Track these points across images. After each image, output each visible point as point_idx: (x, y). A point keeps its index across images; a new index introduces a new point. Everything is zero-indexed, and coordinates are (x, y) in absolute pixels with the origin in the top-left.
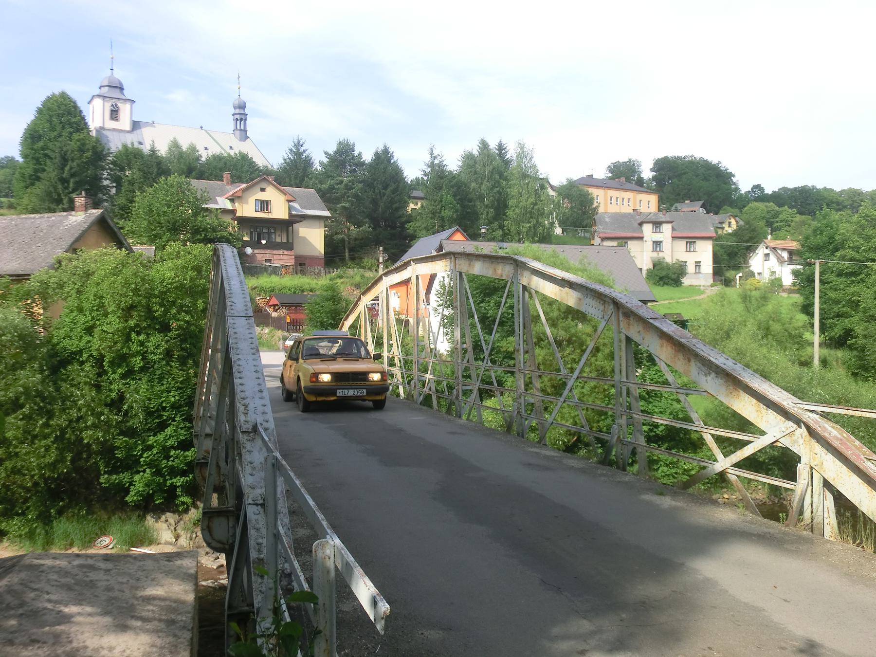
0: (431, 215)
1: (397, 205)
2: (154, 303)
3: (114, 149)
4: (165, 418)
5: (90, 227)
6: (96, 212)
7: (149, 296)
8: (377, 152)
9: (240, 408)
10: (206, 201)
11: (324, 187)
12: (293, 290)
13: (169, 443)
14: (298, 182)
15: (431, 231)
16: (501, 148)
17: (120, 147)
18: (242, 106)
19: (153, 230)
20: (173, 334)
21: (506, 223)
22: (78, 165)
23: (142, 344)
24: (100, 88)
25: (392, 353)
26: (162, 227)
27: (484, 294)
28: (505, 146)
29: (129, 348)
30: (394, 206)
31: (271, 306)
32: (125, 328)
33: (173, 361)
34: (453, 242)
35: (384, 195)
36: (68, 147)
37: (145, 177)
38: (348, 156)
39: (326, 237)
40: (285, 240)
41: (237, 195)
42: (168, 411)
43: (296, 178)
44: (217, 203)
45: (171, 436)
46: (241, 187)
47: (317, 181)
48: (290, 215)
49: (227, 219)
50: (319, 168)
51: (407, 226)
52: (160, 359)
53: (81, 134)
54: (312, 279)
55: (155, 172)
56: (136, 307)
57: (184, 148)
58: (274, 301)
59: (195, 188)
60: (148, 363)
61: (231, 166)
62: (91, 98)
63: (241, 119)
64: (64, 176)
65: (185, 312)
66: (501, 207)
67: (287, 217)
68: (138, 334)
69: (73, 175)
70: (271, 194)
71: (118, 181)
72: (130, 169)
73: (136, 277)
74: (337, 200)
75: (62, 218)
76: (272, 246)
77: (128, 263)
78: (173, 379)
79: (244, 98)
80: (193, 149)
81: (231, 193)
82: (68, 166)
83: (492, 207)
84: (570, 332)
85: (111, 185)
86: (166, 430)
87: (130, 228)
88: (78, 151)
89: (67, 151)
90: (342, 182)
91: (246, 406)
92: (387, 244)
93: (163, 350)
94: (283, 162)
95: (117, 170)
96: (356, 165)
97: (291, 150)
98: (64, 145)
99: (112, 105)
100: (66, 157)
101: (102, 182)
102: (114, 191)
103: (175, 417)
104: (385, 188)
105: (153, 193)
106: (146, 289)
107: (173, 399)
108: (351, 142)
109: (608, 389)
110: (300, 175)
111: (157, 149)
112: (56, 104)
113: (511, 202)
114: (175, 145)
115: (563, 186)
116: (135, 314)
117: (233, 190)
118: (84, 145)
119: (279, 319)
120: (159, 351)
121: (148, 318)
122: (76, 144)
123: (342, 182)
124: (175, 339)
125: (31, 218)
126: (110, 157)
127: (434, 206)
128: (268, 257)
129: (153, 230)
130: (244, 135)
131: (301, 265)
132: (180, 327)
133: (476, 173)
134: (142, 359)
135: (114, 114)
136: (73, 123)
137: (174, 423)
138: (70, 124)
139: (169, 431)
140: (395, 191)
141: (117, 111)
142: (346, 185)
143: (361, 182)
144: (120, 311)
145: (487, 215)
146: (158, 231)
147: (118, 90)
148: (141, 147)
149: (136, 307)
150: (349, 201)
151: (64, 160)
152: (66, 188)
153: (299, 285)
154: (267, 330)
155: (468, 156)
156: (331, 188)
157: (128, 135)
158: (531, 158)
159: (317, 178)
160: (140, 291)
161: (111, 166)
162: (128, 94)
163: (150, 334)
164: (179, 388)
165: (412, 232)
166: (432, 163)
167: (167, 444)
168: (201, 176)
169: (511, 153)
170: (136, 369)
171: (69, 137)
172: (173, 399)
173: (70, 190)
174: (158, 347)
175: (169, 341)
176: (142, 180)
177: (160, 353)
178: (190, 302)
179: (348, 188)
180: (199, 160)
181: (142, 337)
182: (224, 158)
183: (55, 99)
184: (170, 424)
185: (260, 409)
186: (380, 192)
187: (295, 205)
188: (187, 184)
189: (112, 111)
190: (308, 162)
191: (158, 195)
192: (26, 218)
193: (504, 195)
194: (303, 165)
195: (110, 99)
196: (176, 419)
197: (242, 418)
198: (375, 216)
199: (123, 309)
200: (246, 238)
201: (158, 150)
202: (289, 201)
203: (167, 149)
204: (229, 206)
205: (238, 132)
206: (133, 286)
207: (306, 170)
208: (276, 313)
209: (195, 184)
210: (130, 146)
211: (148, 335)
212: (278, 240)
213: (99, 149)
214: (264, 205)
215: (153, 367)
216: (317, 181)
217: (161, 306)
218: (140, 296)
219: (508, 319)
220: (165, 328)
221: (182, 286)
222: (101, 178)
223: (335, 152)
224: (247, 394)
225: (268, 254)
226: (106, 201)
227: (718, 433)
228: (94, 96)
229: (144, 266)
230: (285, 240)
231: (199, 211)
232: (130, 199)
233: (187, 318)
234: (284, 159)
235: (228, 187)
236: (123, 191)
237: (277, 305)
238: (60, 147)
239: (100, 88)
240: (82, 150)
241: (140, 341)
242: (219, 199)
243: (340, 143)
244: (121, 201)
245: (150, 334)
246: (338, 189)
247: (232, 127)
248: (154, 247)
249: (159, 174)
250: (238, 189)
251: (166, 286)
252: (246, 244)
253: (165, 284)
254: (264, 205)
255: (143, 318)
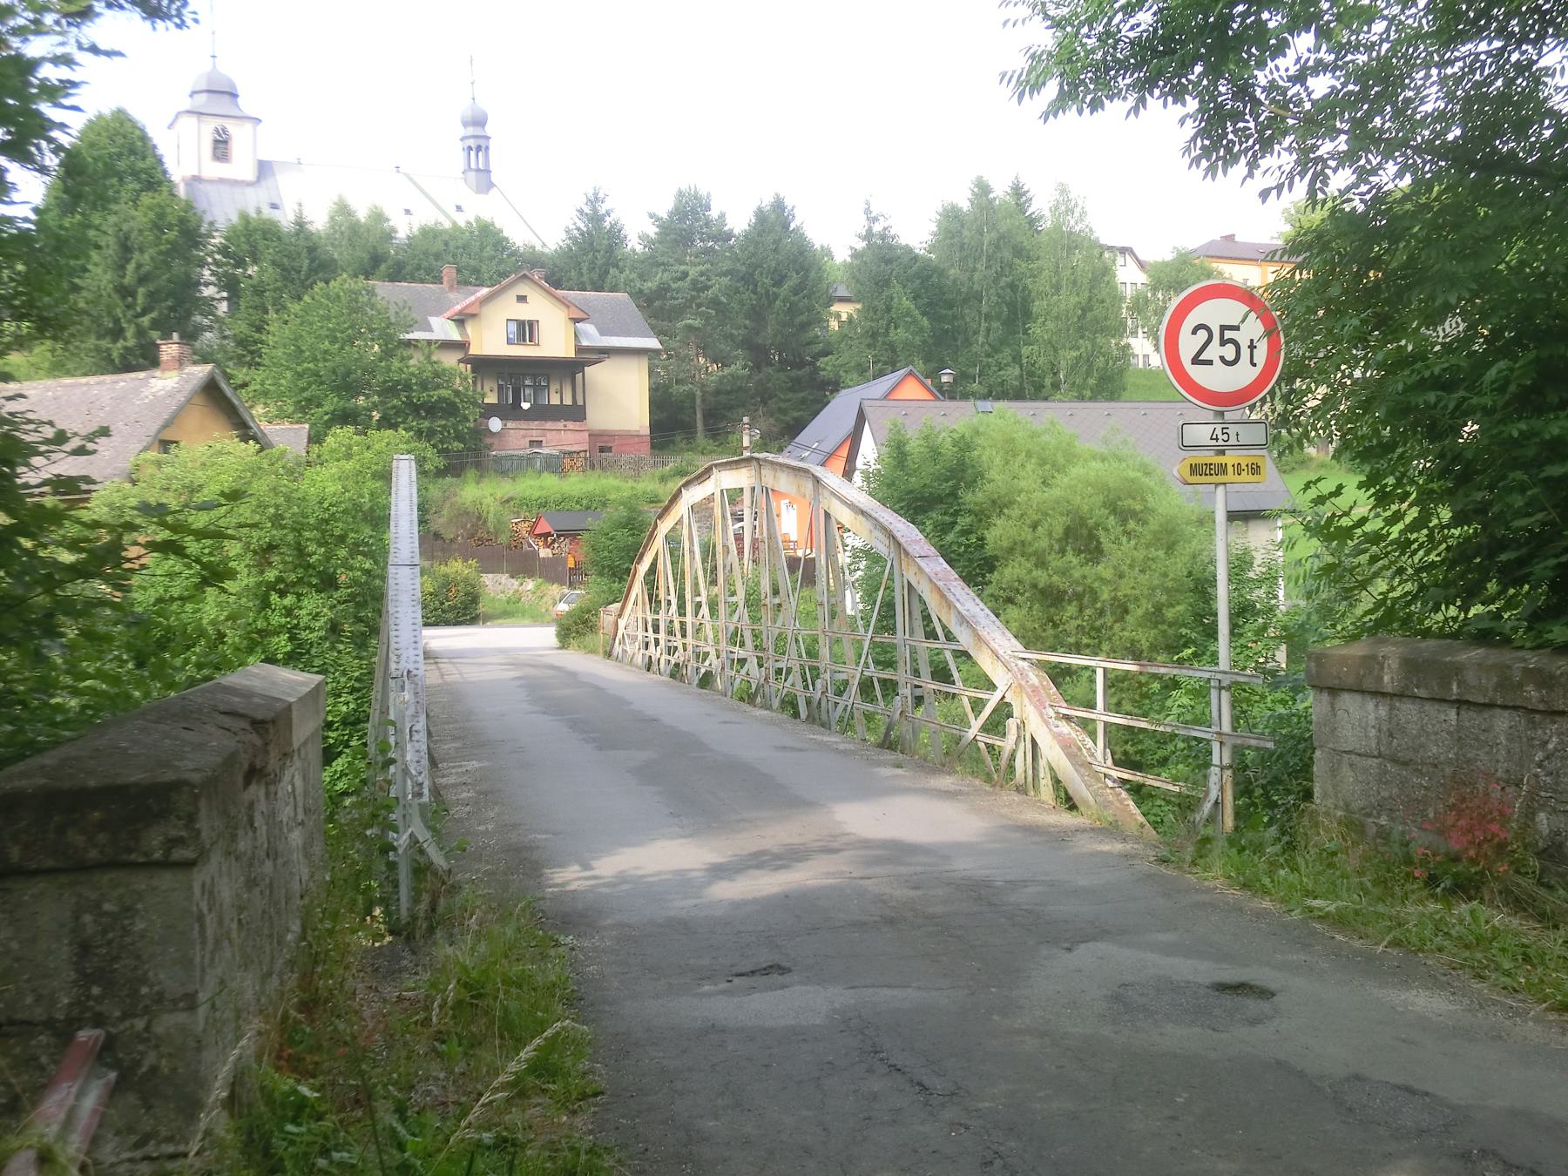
0: (869, 340)
1: (803, 318)
2: (308, 539)
3: (222, 224)
4: (332, 741)
5: (189, 401)
6: (201, 371)
7: (298, 529)
8: (759, 209)
9: (393, 658)
10: (409, 327)
11: (649, 285)
12: (584, 502)
13: (341, 786)
14: (595, 277)
15: (864, 373)
16: (1018, 191)
17: (235, 219)
18: (479, 121)
19: (304, 390)
20: (342, 593)
21: (1025, 351)
22: (152, 259)
23: (289, 612)
24: (191, 96)
25: (700, 616)
26: (322, 383)
27: (915, 509)
28: (1025, 188)
29: (267, 619)
30: (798, 320)
31: (540, 535)
32: (259, 584)
33: (342, 642)
34: (892, 403)
35: (775, 299)
36: (132, 224)
37: (285, 278)
38: (697, 220)
39: (650, 389)
40: (568, 401)
41: (469, 311)
42: (337, 729)
43: (591, 270)
44: (429, 329)
45: (343, 774)
46: (479, 294)
47: (634, 276)
48: (580, 350)
49: (450, 360)
50: (639, 249)
51: (823, 360)
52: (321, 638)
53: (156, 195)
54: (625, 479)
55: (304, 268)
56: (276, 547)
57: (362, 215)
58: (544, 527)
59: (384, 303)
60: (300, 646)
61: (457, 248)
62: (173, 117)
63: (479, 148)
64: (126, 281)
65: (364, 554)
66: (1017, 313)
67: (573, 355)
68: (282, 594)
69: (143, 280)
70: (542, 308)
71: (231, 286)
72: (255, 262)
73: (276, 495)
74: (678, 312)
75: (137, 383)
76: (544, 413)
77: (260, 468)
78: (344, 673)
79: (484, 104)
80: (378, 217)
81: (458, 307)
82: (133, 261)
83: (998, 317)
84: (1071, 576)
85: (218, 296)
86: (334, 764)
87: (258, 387)
88: (151, 230)
89: (131, 230)
90: (685, 275)
91: (398, 656)
92: (786, 401)
93: (326, 623)
94: (564, 236)
95: (229, 264)
96: (715, 238)
97: (581, 212)
98: (125, 220)
99: (217, 130)
100: (129, 244)
101: (199, 291)
102: (223, 307)
103: (348, 740)
104: (778, 283)
105: (301, 313)
106: (294, 514)
107: (344, 708)
108: (703, 192)
109: (1147, 683)
110: (599, 262)
111: (308, 219)
112: (104, 134)
113: (1037, 306)
114: (343, 209)
115: (1166, 264)
116: (275, 559)
117: (462, 301)
118: (161, 216)
119: (557, 561)
120: (318, 624)
121: (300, 566)
122: (146, 215)
123: (685, 275)
124: (345, 602)
125: (81, 385)
126: (214, 237)
127: (872, 320)
128: (535, 436)
129: (304, 390)
130: (483, 180)
131: (602, 450)
132: (355, 582)
133: (962, 247)
134: (291, 639)
135: (221, 147)
136: (139, 172)
137: (347, 751)
138: (135, 174)
139: (339, 764)
140: (796, 291)
141: (226, 142)
142: (694, 282)
143: (725, 274)
144: (250, 555)
145: (987, 336)
146: (313, 391)
147: (227, 97)
148: (276, 215)
149: (276, 547)
150: (701, 315)
151: (126, 248)
152: (129, 307)
153: (597, 492)
154: (530, 585)
155: (948, 212)
156: (663, 291)
157: (250, 191)
158: (1083, 213)
159: (633, 268)
160: (283, 519)
161: (218, 257)
162: (246, 104)
163: (302, 595)
164: (353, 690)
165: (831, 375)
166: (870, 230)
167: (337, 788)
168: (396, 275)
169: (1041, 204)
170: (280, 656)
171: (134, 202)
172: (344, 708)
173: (139, 309)
174: (316, 617)
175: (335, 606)
176: (279, 284)
177: (321, 628)
178: (371, 537)
179: (698, 287)
180: (392, 238)
181: (289, 600)
182: (446, 231)
183: (103, 123)
184: (340, 753)
185: (413, 658)
186: (768, 291)
187: (588, 328)
188: (368, 293)
189: (216, 142)
190: (614, 237)
191: (311, 319)
192: (72, 386)
193: (1023, 290)
194: (605, 242)
195: (210, 119)
196: (352, 744)
197: (393, 666)
198: (760, 341)
199: (255, 553)
200: (492, 399)
201: (311, 222)
202: (576, 321)
203: (326, 219)
204: (454, 335)
205: (472, 175)
206: (272, 510)
207: (612, 252)
208: (548, 550)
209: (385, 291)
210: (254, 215)
211: (299, 596)
212: (555, 400)
213: (193, 224)
214: (526, 330)
215: (308, 652)
216: (634, 276)
217: (320, 545)
218: (283, 527)
219: (959, 555)
220: (328, 583)
221: (357, 507)
222: (199, 284)
223: (671, 214)
224: (400, 645)
225: (534, 429)
226: (210, 328)
227: (973, 694)
228: (179, 113)
229: (290, 472)
230: (568, 401)
231: (395, 347)
232: (257, 323)
233: (367, 566)
234: (568, 231)
235: (451, 296)
236: (242, 307)
237: (549, 534)
238: (116, 225)
239: (191, 96)
240: (158, 226)
241: (285, 607)
242: (435, 321)
243: (680, 194)
244: (242, 328)
245: (302, 595)
246: (678, 290)
247: (460, 163)
248: (307, 426)
249: (313, 271)
250: (473, 298)
251: (328, 509)
252: (491, 411)
253: (325, 505)
254: (526, 330)
255: (290, 566)
